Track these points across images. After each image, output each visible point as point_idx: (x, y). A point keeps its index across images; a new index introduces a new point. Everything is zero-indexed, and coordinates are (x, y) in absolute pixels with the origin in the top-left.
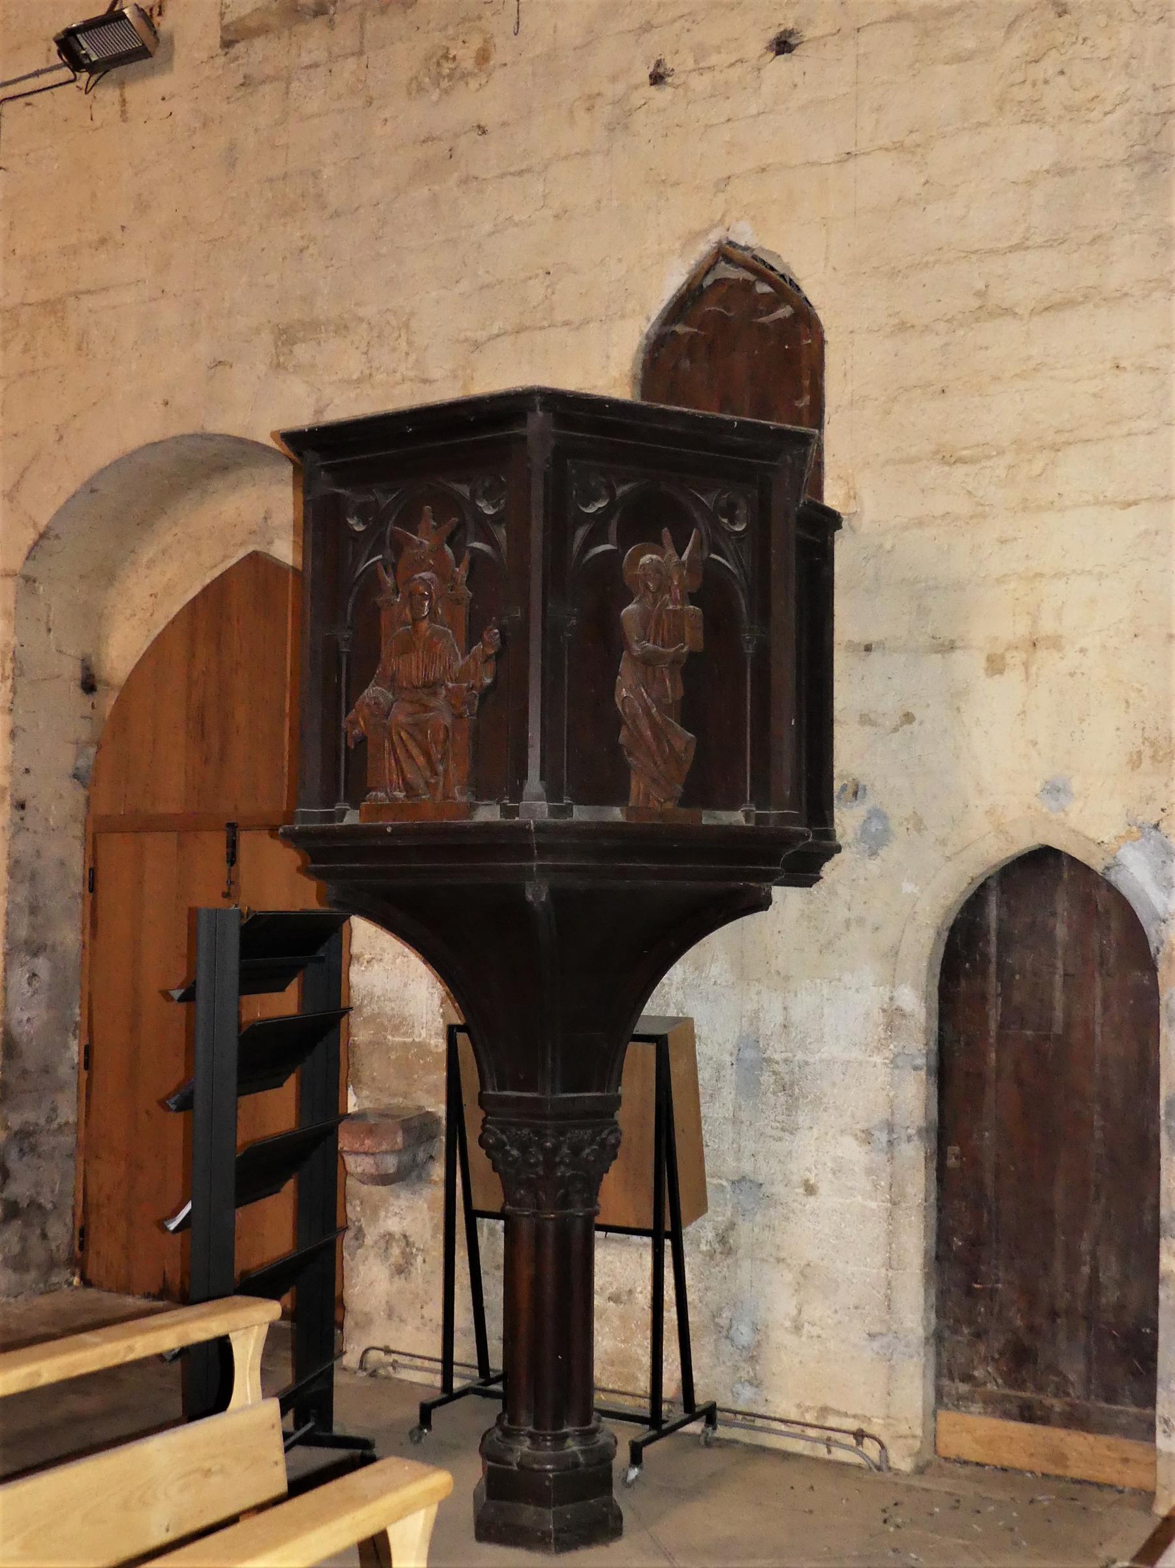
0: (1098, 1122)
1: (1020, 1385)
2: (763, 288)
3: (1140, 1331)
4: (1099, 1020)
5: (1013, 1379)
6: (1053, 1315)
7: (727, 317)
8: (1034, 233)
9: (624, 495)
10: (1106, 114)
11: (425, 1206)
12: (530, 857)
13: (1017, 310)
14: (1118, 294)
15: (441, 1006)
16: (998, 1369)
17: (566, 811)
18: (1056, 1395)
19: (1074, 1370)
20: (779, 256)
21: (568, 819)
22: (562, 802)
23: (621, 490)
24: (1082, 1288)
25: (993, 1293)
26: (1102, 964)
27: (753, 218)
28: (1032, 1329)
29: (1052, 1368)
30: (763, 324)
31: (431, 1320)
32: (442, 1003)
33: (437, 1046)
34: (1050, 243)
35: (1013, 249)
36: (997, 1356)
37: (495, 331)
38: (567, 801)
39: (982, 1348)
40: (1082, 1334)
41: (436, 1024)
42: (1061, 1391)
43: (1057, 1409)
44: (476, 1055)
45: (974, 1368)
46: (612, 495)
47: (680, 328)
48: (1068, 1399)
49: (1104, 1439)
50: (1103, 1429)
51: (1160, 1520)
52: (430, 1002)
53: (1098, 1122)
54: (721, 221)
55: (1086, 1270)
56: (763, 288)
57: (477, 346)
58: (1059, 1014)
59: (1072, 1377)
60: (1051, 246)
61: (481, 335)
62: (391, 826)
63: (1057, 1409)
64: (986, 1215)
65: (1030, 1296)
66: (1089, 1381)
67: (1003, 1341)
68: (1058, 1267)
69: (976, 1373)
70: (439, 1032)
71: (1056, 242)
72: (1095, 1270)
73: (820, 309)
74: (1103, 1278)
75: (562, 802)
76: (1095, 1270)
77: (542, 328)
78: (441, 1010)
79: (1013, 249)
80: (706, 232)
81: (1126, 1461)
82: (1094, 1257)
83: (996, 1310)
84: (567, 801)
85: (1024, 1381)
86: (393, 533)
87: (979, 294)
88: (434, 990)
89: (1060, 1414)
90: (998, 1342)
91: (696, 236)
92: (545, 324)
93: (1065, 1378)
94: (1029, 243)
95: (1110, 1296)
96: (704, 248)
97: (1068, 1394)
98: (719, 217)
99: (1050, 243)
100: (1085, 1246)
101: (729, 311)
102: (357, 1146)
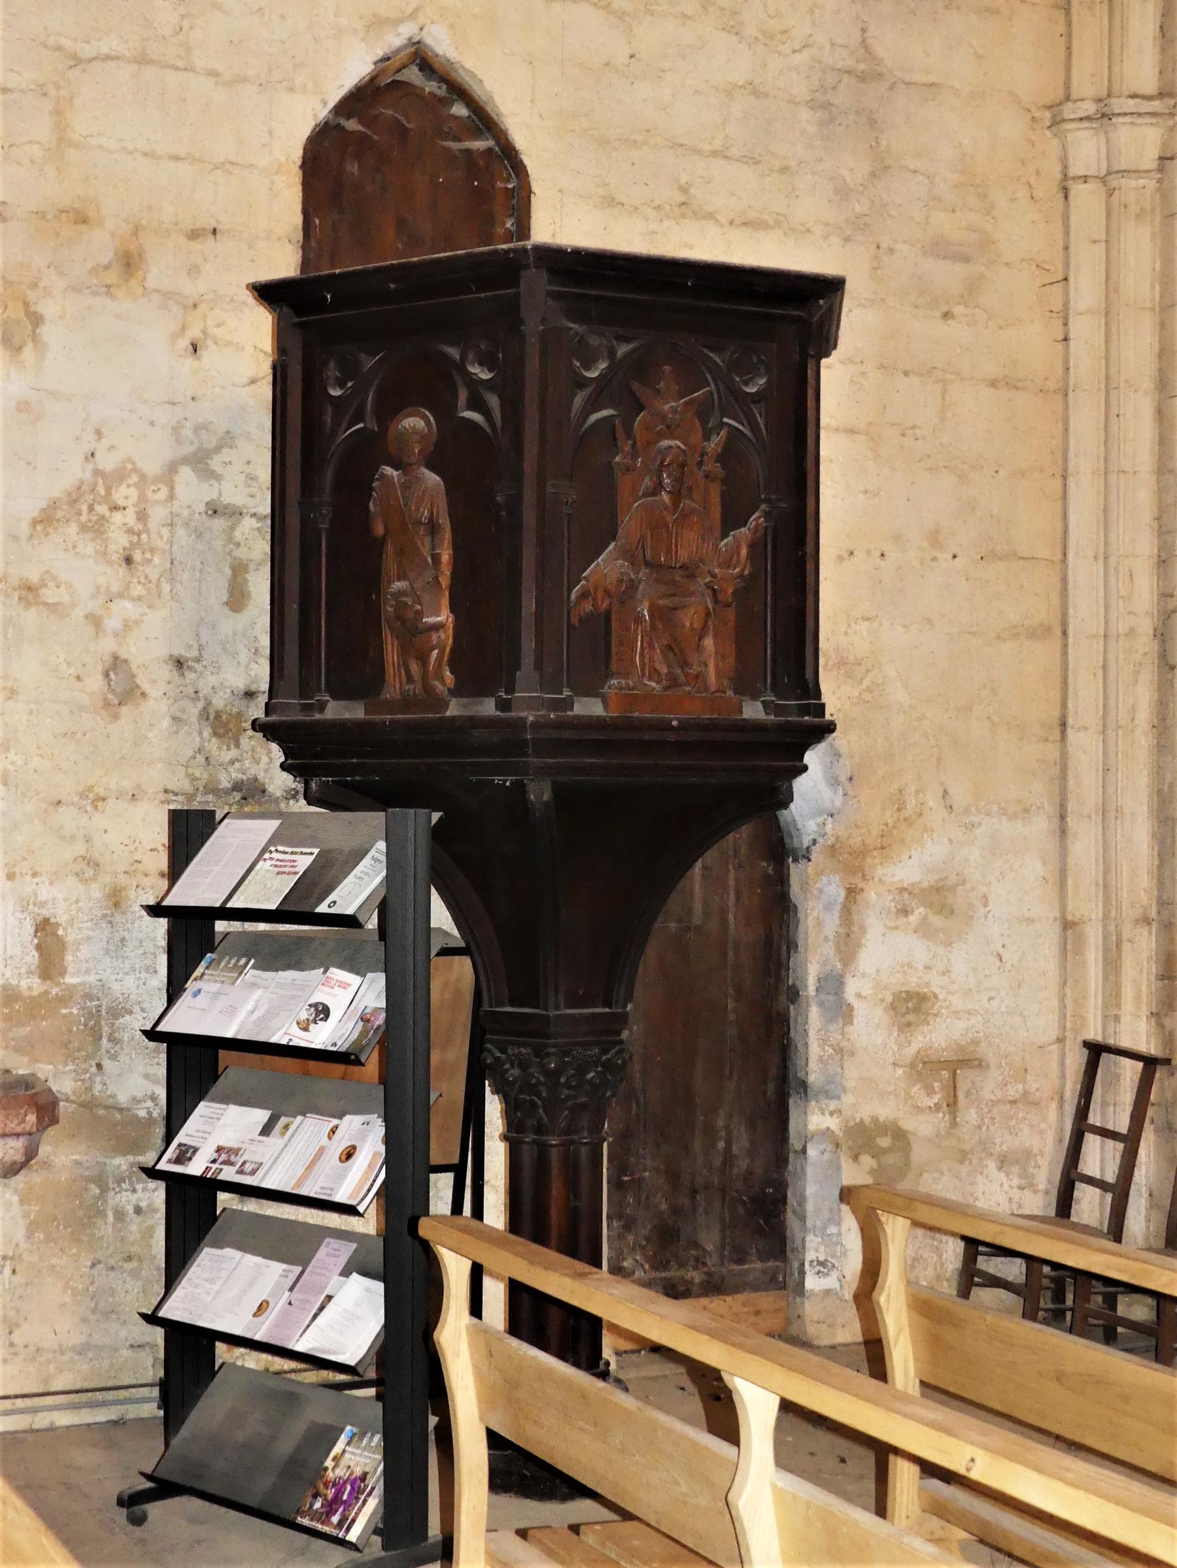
0: (731, 1004)
1: (664, 1265)
2: (460, 110)
3: (765, 1192)
4: (732, 909)
5: (658, 1263)
6: (694, 1192)
7: (406, 128)
8: (732, 145)
9: (627, 355)
10: (794, 51)
11: (16, 1198)
12: (525, 755)
13: (718, 217)
14: (801, 228)
15: (35, 936)
16: (645, 1255)
17: (568, 704)
18: (695, 1268)
19: (710, 1239)
20: (481, 81)
21: (569, 713)
22: (562, 694)
23: (623, 349)
24: (717, 1163)
25: (641, 1180)
26: (735, 855)
27: (452, 26)
28: (676, 1210)
29: (696, 1245)
30: (449, 149)
31: (26, 1347)
32: (36, 932)
33: (30, 988)
34: (746, 160)
35: (715, 154)
36: (644, 1243)
37: (105, 50)
38: (567, 693)
39: (630, 1238)
40: (717, 1206)
41: (29, 959)
42: (699, 1262)
43: (697, 1280)
44: (429, 989)
45: (624, 1259)
46: (612, 353)
47: (352, 125)
48: (705, 1269)
49: (741, 1297)
50: (736, 1289)
51: (862, 1347)
52: (17, 931)
53: (731, 1004)
54: (413, 15)
55: (721, 1145)
56: (460, 110)
57: (77, 61)
58: (698, 906)
59: (709, 1247)
60: (747, 163)
61: (87, 51)
62: (677, 719)
63: (697, 1280)
64: (634, 1106)
65: (673, 1176)
66: (723, 1247)
67: (649, 1227)
68: (697, 1145)
69: (625, 1264)
70: (33, 968)
71: (751, 160)
72: (729, 1144)
73: (315, 115)
74: (735, 1149)
75: (562, 694)
76: (729, 1144)
77: (177, 68)
78: (36, 941)
79: (715, 154)
80: (398, 22)
81: (757, 1313)
82: (727, 1128)
83: (643, 1199)
84: (567, 693)
85: (668, 1262)
86: (709, 385)
87: (684, 190)
88: (25, 914)
89: (701, 1283)
90: (644, 1229)
91: (377, 24)
92: (181, 64)
93: (704, 1250)
94: (728, 153)
95: (742, 1164)
96: (395, 39)
97: (704, 1264)
98: (410, 10)
99: (746, 160)
100: (720, 1123)
101: (408, 122)
102: (13, 1125)
